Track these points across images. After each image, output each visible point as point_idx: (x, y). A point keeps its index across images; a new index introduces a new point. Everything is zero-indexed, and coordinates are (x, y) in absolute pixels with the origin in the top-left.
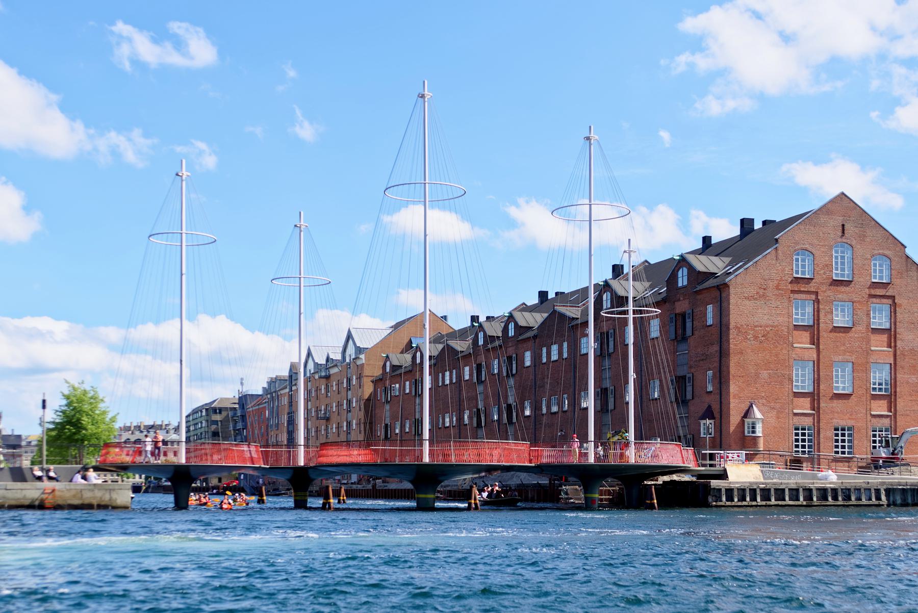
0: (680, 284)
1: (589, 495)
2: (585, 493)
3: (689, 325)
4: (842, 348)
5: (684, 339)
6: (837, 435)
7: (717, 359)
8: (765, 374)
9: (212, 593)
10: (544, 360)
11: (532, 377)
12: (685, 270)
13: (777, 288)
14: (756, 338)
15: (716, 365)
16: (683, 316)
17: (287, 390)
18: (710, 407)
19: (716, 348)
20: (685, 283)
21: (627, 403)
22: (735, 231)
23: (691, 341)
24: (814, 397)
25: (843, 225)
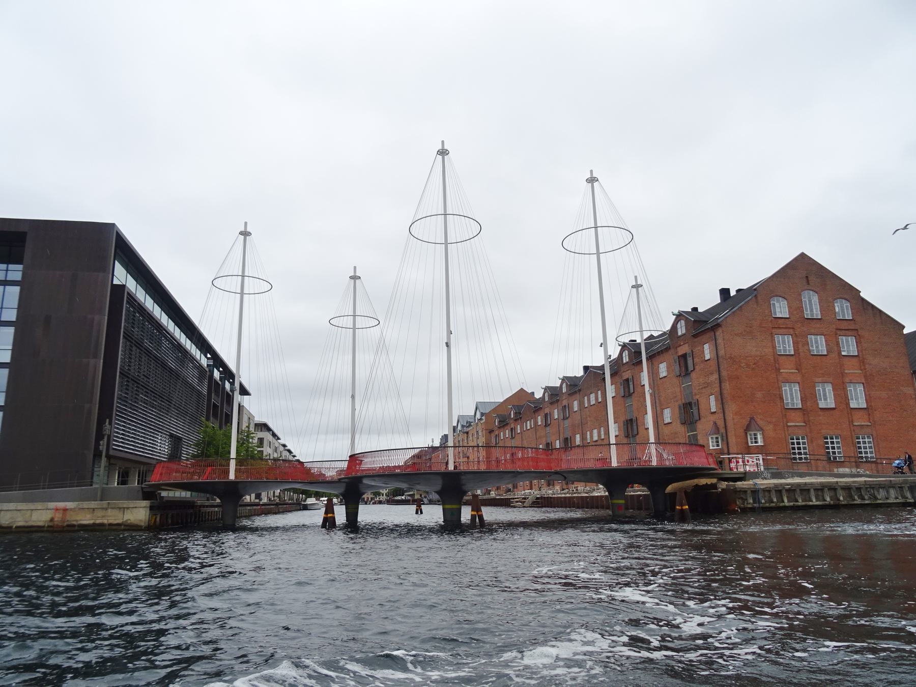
0: (680, 334)
7: (717, 385)
8: (759, 395)
9: (171, 583)
12: (683, 322)
14: (748, 365)
15: (718, 389)
18: (715, 423)
19: (716, 376)
20: (684, 331)
21: (648, 429)
23: (693, 375)
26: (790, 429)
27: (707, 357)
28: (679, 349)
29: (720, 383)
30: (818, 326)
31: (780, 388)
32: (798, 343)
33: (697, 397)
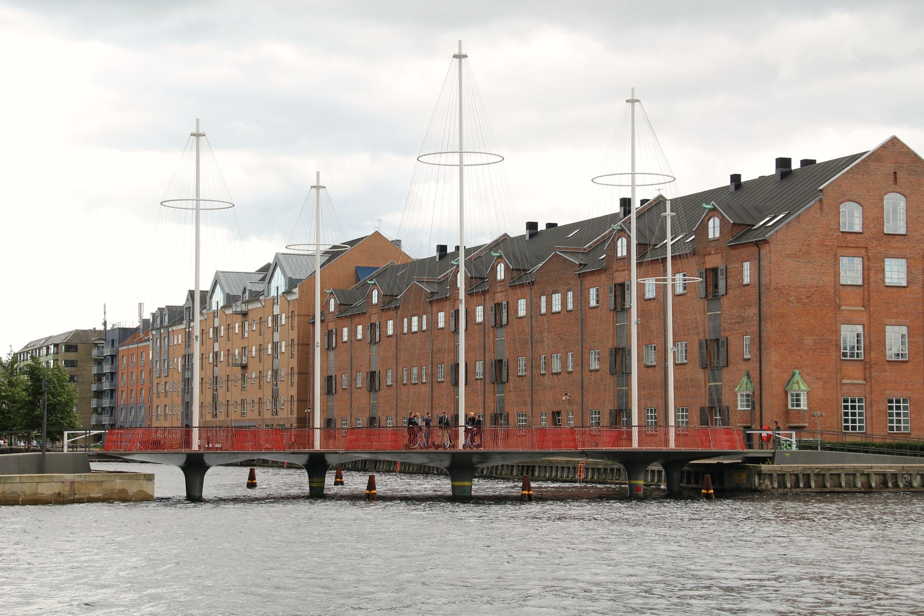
1: (634, 482)
2: (630, 479)
3: (722, 283)
4: (895, 310)
5: (716, 297)
6: (891, 408)
7: (756, 323)
8: (809, 341)
10: (543, 310)
11: (528, 330)
12: (717, 221)
13: (822, 244)
14: (799, 300)
15: (756, 329)
16: (715, 270)
17: (183, 326)
19: (754, 310)
20: (717, 235)
22: (770, 170)
23: (725, 301)
24: (867, 365)
25: (895, 173)
26: (844, 387)
27: (747, 280)
28: (708, 258)
29: (760, 320)
30: (900, 245)
31: (838, 332)
32: (869, 270)
33: (727, 334)
